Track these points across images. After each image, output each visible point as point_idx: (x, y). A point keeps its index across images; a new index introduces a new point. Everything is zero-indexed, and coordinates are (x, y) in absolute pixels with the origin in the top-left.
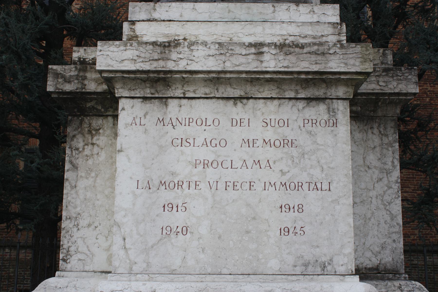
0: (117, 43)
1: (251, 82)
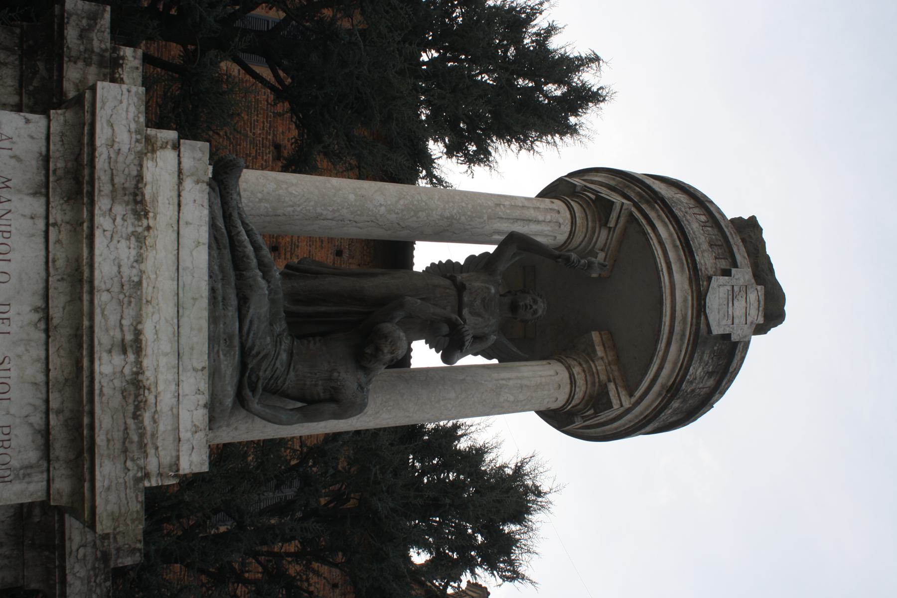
0: (142, 119)
1: (76, 336)
